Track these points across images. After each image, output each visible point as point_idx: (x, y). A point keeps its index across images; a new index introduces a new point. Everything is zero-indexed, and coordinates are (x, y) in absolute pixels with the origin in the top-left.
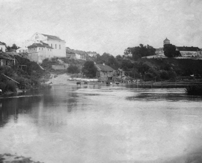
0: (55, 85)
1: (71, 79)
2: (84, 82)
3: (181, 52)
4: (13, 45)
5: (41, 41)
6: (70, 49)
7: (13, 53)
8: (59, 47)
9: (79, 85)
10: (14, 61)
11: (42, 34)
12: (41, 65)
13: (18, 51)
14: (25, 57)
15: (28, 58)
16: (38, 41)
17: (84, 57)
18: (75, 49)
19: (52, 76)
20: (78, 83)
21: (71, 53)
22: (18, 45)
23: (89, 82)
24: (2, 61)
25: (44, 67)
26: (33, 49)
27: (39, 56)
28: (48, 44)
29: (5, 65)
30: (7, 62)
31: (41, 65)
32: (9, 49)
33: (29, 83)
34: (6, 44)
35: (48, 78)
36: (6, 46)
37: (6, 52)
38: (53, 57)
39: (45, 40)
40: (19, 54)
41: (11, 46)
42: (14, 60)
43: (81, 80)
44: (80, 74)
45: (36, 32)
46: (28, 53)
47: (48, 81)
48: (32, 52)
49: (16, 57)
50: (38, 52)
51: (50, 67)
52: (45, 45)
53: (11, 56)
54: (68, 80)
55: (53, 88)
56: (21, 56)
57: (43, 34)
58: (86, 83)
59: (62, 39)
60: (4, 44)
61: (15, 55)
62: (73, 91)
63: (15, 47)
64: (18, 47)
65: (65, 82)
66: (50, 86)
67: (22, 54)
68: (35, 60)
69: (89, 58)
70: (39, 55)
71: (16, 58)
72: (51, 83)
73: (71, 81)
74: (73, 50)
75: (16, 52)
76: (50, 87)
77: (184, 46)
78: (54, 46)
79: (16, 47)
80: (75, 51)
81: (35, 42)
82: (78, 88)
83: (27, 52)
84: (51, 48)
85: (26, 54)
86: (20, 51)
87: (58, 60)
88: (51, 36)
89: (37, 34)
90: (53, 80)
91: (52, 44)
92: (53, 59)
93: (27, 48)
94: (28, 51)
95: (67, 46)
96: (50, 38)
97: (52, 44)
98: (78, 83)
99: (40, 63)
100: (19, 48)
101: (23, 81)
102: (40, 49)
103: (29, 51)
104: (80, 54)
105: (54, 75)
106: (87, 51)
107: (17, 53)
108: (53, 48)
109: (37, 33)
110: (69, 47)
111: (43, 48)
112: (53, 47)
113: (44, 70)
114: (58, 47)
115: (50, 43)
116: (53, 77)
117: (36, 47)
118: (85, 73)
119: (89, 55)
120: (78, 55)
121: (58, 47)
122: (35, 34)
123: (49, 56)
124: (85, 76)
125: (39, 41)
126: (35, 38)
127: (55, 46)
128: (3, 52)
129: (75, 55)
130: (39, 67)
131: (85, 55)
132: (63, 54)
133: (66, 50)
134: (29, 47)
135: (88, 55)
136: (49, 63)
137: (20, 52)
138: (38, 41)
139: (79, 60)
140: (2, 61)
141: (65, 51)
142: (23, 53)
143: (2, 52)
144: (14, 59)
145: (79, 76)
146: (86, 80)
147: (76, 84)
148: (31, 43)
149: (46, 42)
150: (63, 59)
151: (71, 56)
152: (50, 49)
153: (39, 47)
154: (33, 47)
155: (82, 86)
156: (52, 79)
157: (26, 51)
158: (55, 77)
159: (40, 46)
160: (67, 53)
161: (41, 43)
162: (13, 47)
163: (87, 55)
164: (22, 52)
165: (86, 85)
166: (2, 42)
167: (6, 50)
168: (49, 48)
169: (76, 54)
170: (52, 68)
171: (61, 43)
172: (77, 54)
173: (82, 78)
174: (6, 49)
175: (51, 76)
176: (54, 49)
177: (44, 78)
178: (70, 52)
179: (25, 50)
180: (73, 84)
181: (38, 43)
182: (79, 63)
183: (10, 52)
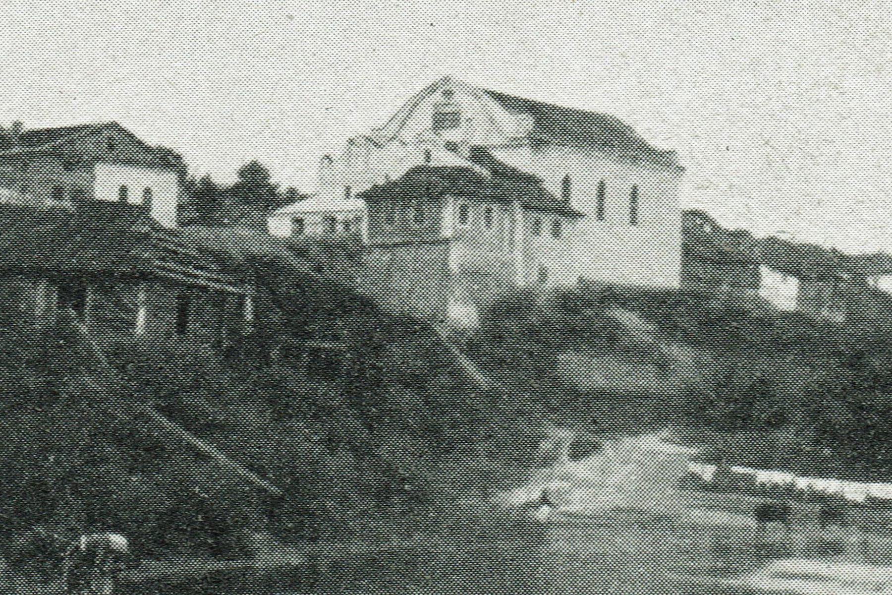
0: (573, 521)
1: (708, 472)
2: (818, 507)
3: (764, 270)
4: (242, 173)
5: (479, 154)
6: (716, 228)
7: (236, 237)
8: (608, 200)
9: (775, 532)
10: (248, 302)
11: (500, 98)
12: (472, 349)
13: (280, 226)
14: (339, 271)
15: (362, 285)
16: (452, 147)
17: (828, 292)
18: (760, 232)
19: (558, 445)
20: (764, 514)
21: (723, 260)
22: (282, 178)
23: (856, 505)
24: (142, 296)
25: (490, 365)
26: (411, 214)
27: (462, 274)
28: (531, 180)
29: (168, 335)
30: (183, 312)
31: (472, 349)
32: (203, 200)
33: (364, 490)
34: (187, 160)
35: (525, 458)
36: (182, 172)
37: (182, 224)
38: (570, 282)
39: (514, 144)
40: (291, 247)
41: (226, 176)
42: (242, 297)
43: (790, 490)
44: (785, 437)
45: (445, 71)
46: (365, 240)
47: (520, 482)
48: (397, 240)
49: (263, 271)
50: (446, 241)
51: (544, 370)
52: (493, 186)
53: (221, 259)
54: (692, 481)
55: (559, 543)
56: (304, 267)
57: (498, 90)
58: (832, 510)
59: (658, 143)
60: (166, 160)
61: (252, 259)
62: (726, 572)
63: (256, 190)
64: (283, 189)
65: (662, 499)
66: (538, 524)
67: (314, 250)
68: (422, 308)
69: (873, 311)
70: (454, 265)
71: (260, 281)
72: (544, 500)
73: (706, 488)
74: (740, 235)
75: (266, 231)
76: (527, 530)
77: (17, 125)
78: (582, 199)
79: (272, 190)
80: (757, 243)
81: (428, 157)
82: (767, 552)
83: (357, 238)
84: (563, 211)
85: (353, 251)
86: (299, 222)
87: (608, 313)
88: (554, 108)
89: (448, 94)
90: (565, 478)
91: (566, 182)
92: (567, 302)
93: (361, 204)
94: (364, 227)
95: (688, 197)
96: (551, 124)
97: (566, 182)
98: (764, 514)
99: (463, 333)
100: (293, 196)
101: (307, 469)
102: (471, 214)
103: (371, 226)
104: (797, 273)
105: (566, 435)
106: (853, 242)
107: (275, 241)
108: (576, 215)
109: (446, 80)
110: (713, 214)
111: (495, 207)
112: (575, 204)
113: (493, 397)
114: (617, 204)
115: (550, 167)
116: (565, 451)
117: (436, 197)
118: (827, 433)
119: (870, 281)
120: (778, 276)
121: (617, 204)
122: (432, 89)
123: (543, 275)
124: (827, 451)
125: (466, 153)
126: (429, 123)
127: (627, 199)
128: (156, 227)
129: (757, 275)
130: (453, 360)
131: (838, 279)
132: (665, 273)
133: (685, 231)
134: (373, 197)
135: (863, 283)
136: (544, 336)
137: (300, 231)
138: (452, 147)
139: (785, 316)
140: (142, 296)
141: (678, 240)
142: (327, 246)
143: (145, 229)
144: (249, 290)
145: (777, 456)
146: (830, 486)
147: (752, 522)
148: (393, 165)
149: (521, 160)
150: (651, 302)
151: (725, 288)
152: (547, 221)
153: (461, 201)
154: (411, 196)
155: (799, 538)
156: (558, 469)
157: (347, 225)
158: (579, 452)
159: (470, 195)
160: (687, 252)
161: (477, 168)
162: (237, 186)
163: (859, 279)
164: (314, 229)
165: (834, 532)
166: (152, 141)
167: (180, 208)
168: (545, 210)
169: (764, 270)
170: (560, 371)
171: (642, 176)
172: (775, 267)
173: (804, 474)
174: (186, 199)
175: (545, 446)
176: (581, 224)
177: (491, 455)
178: (711, 250)
179: (340, 218)
180: (720, 518)
181: (445, 159)
182: (780, 346)
183: (217, 230)
